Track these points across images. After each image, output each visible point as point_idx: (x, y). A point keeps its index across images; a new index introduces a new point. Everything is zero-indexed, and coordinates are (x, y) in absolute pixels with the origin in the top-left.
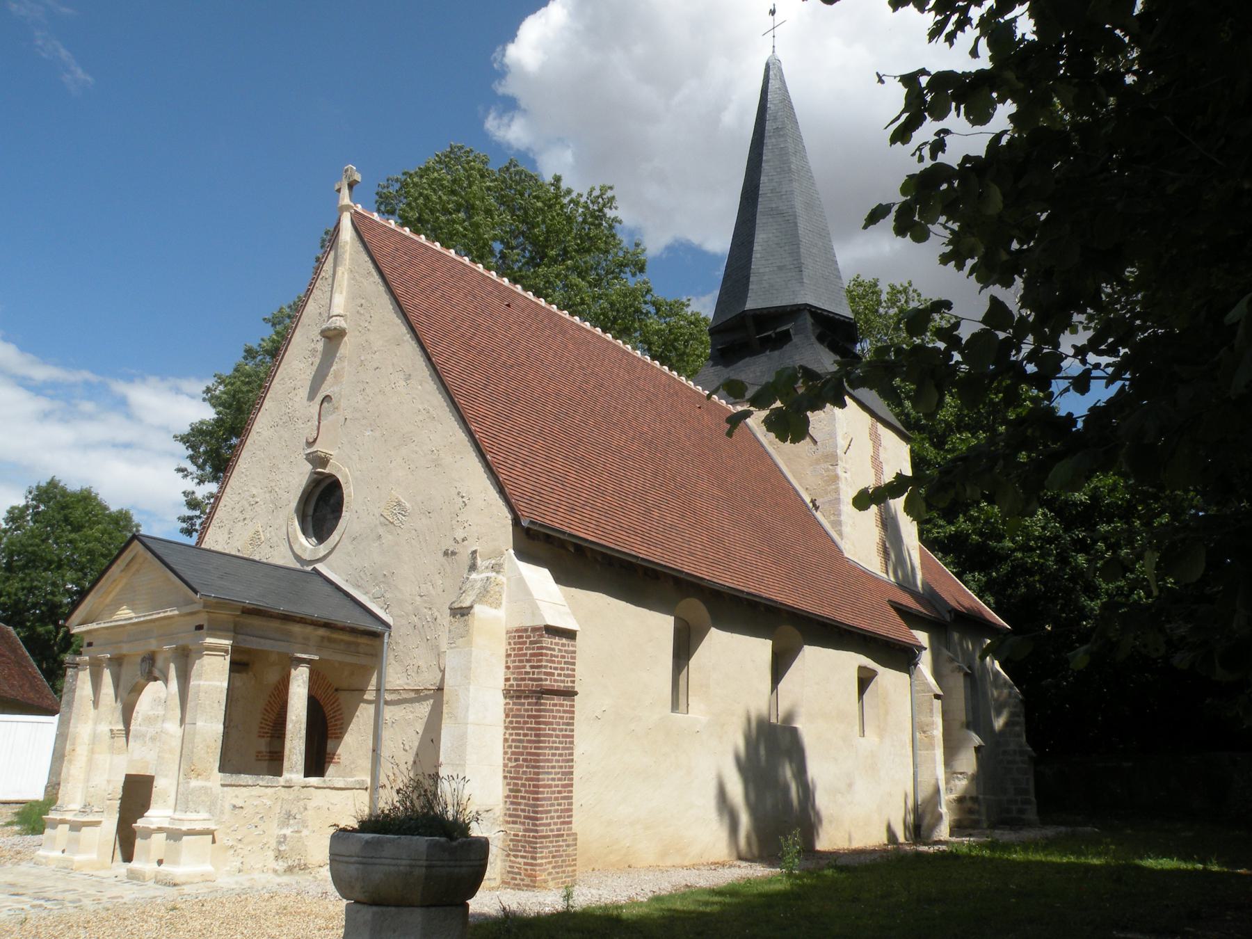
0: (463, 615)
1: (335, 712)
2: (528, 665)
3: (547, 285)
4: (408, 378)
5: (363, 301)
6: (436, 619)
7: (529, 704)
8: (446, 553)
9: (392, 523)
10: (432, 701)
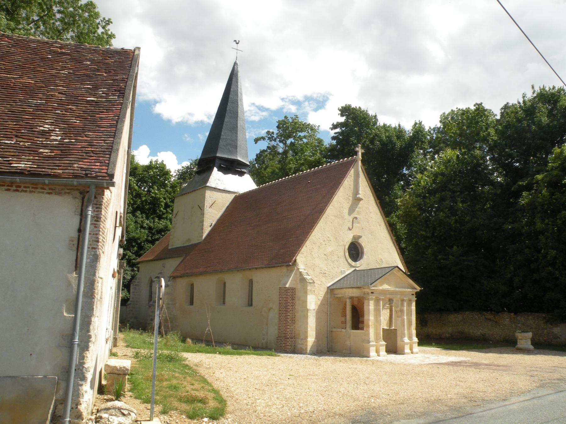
4: (380, 225)
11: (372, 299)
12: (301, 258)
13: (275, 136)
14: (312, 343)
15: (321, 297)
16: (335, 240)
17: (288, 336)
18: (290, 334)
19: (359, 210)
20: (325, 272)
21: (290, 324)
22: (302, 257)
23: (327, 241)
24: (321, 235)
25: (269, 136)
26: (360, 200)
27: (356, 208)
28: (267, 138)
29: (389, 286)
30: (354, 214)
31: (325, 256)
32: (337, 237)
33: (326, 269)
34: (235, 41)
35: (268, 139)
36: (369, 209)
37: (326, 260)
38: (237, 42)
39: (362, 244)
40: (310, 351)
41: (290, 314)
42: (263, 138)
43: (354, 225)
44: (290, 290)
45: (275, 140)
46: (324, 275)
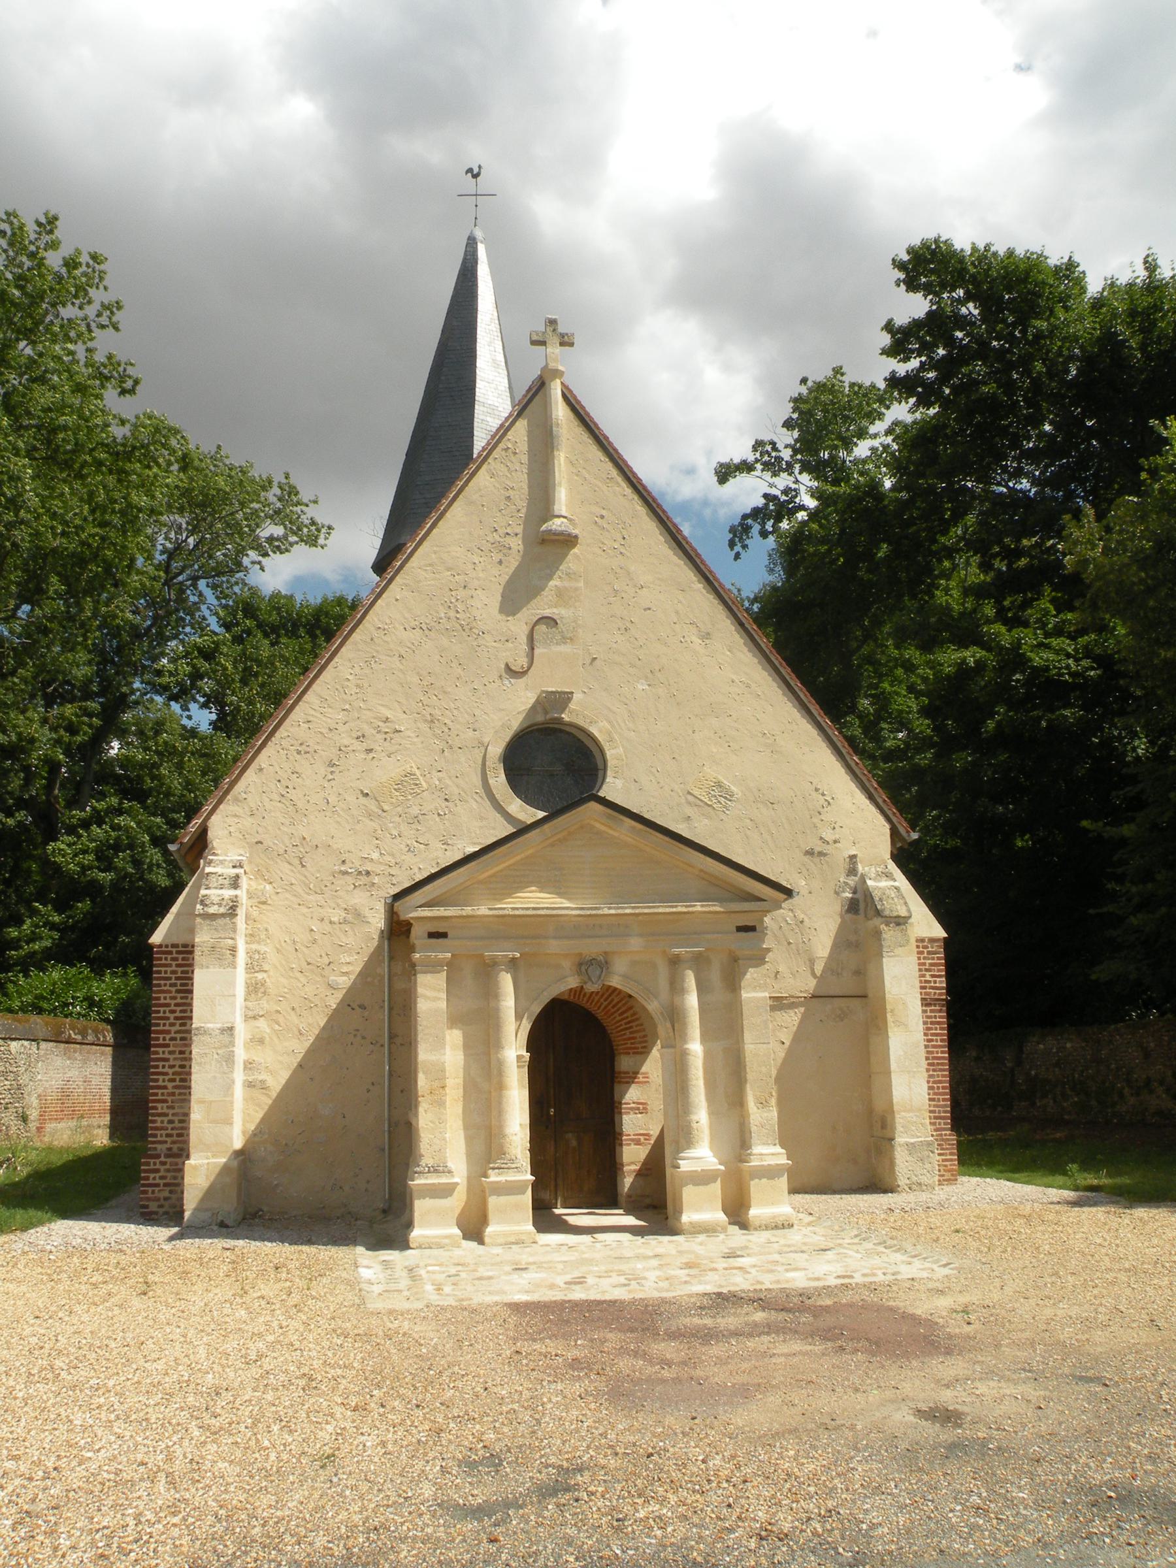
0: (898, 924)
1: (629, 1022)
2: (928, 974)
3: (72, 334)
4: (706, 636)
5: (604, 513)
6: (802, 922)
7: (931, 1011)
8: (810, 853)
9: (709, 806)
10: (802, 1010)
11: (433, 967)
12: (230, 820)
13: (786, 454)
14: (212, 1178)
15: (346, 974)
16: (424, 727)
17: (159, 1146)
18: (168, 1135)
19: (566, 584)
20: (369, 867)
21: (173, 1094)
22: (236, 816)
23: (380, 737)
24: (341, 716)
25: (766, 458)
26: (567, 541)
27: (550, 577)
28: (759, 466)
29: (560, 895)
30: (542, 606)
31: (363, 800)
32: (437, 712)
33: (375, 856)
34: (470, 170)
35: (763, 470)
36: (629, 573)
37: (370, 815)
38: (476, 171)
39: (594, 731)
40: (196, 1210)
41: (170, 1053)
42: (746, 467)
43: (537, 651)
44: (170, 953)
45: (789, 468)
46: (364, 879)
